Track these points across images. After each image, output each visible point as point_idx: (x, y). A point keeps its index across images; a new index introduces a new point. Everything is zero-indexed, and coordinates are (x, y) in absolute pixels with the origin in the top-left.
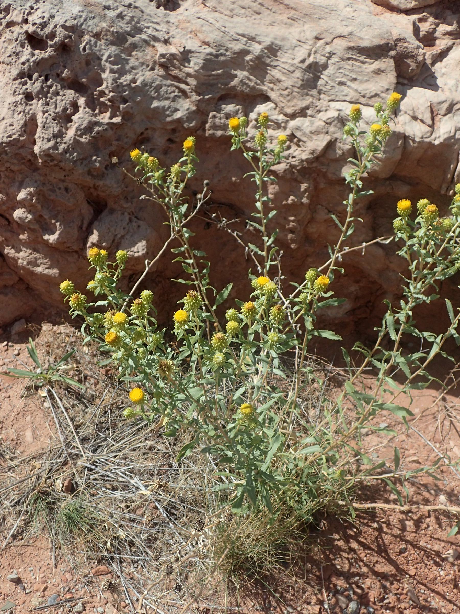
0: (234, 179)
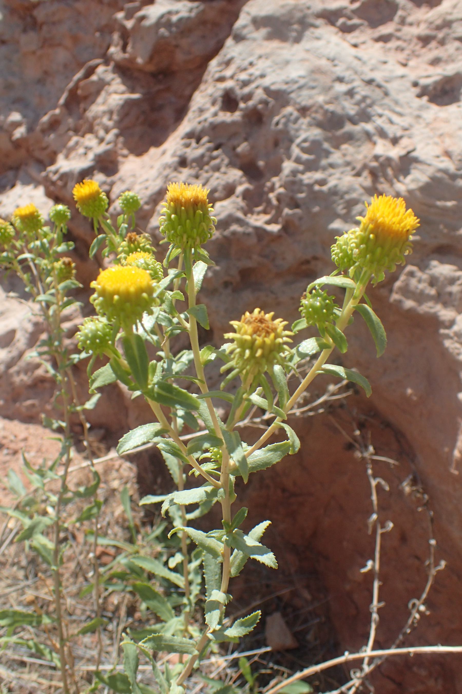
0: (409, 391)
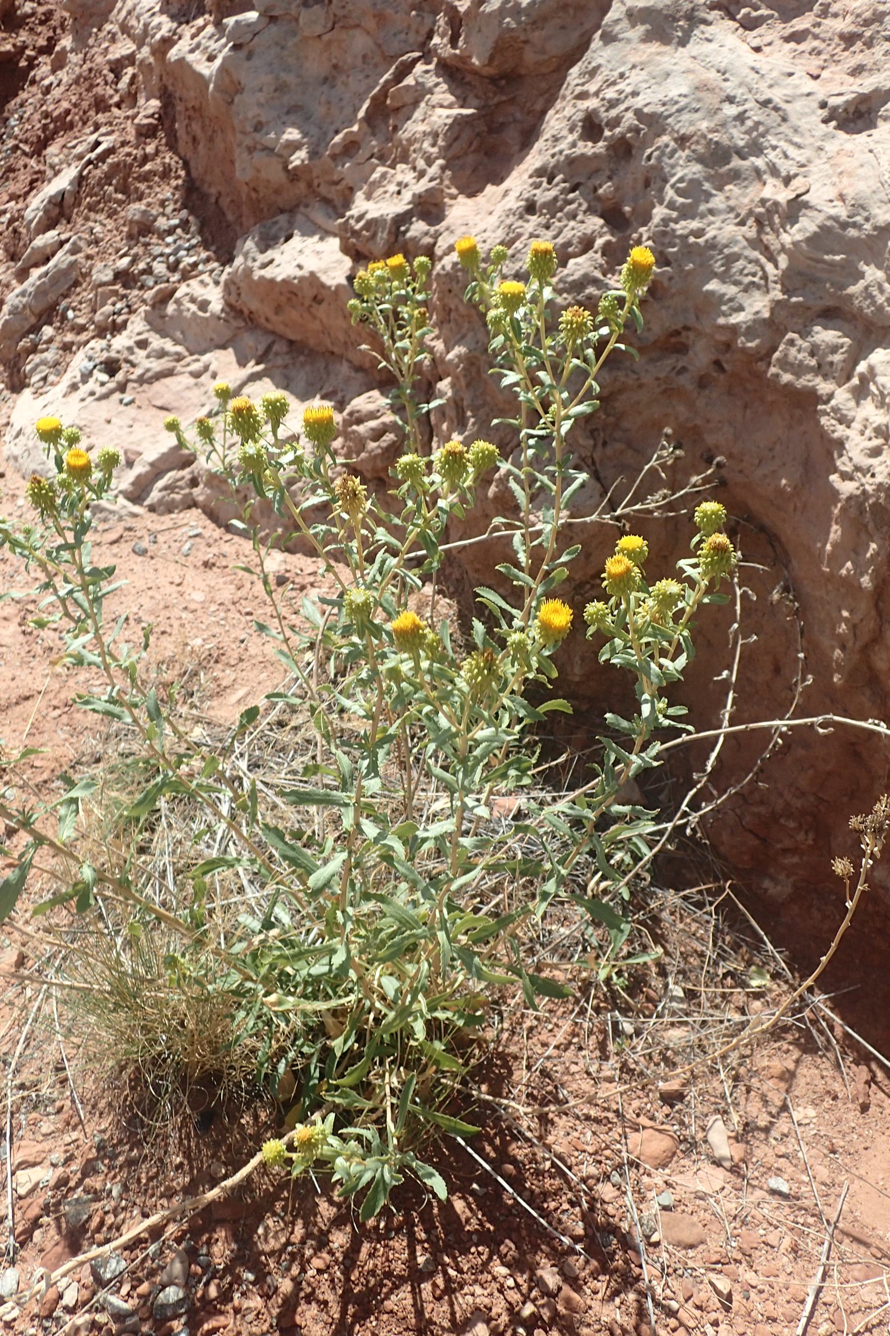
0: (784, 482)
